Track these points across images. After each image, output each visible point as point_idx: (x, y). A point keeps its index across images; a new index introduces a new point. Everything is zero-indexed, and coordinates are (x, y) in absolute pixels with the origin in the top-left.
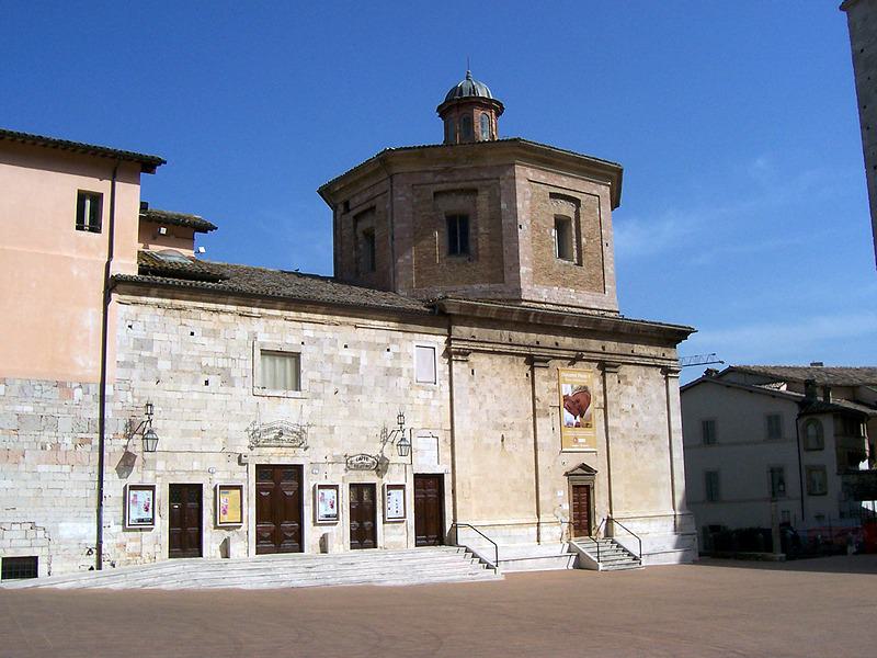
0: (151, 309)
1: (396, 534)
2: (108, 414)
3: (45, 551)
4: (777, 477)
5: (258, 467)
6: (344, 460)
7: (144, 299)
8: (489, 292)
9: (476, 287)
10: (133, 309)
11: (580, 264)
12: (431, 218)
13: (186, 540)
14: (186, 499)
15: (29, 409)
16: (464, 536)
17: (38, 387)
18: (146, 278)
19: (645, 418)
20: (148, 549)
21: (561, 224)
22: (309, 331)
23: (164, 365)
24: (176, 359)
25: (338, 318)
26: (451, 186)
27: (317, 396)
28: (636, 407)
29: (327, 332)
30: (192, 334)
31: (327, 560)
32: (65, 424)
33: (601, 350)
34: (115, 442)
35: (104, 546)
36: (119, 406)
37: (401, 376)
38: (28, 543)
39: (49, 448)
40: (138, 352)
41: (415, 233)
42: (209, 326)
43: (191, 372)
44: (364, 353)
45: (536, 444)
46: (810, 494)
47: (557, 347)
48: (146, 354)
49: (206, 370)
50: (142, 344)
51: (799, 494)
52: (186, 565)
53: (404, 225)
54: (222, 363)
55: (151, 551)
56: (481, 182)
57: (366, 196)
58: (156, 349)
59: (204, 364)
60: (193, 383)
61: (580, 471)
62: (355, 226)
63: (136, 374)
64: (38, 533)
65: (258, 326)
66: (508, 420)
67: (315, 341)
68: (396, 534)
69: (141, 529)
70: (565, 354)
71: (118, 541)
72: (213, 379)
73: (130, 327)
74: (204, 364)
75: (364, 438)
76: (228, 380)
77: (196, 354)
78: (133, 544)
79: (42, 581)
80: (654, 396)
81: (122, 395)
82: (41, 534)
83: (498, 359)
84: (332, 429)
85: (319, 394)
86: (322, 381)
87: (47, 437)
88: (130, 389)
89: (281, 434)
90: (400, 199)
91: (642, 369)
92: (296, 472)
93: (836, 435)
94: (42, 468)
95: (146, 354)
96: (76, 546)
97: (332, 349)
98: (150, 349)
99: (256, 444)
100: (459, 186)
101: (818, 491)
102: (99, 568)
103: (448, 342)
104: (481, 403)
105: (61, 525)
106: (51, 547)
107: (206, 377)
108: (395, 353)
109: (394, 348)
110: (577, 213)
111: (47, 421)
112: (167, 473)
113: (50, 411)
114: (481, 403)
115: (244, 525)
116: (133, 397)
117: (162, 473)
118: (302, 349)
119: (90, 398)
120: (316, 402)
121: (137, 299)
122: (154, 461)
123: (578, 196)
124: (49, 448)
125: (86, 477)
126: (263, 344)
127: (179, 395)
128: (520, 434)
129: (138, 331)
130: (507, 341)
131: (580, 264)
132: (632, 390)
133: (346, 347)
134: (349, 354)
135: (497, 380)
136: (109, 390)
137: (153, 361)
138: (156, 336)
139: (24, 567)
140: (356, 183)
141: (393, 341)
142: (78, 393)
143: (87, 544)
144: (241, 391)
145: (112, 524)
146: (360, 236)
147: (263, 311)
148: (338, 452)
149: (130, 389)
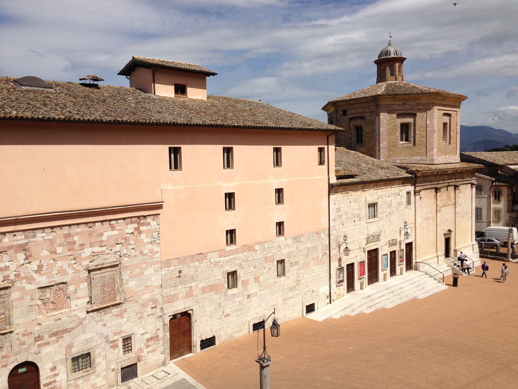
8: (420, 161)
9: (414, 158)
11: (450, 144)
14: (14, 236)
16: (422, 267)
19: (465, 206)
21: (445, 124)
23: (344, 217)
24: (346, 213)
26: (405, 112)
32: (320, 249)
38: (311, 298)
42: (355, 197)
45: (437, 224)
57: (360, 110)
67: (381, 196)
72: (356, 219)
82: (315, 293)
83: (427, 191)
91: (465, 185)
93: (508, 195)
94: (315, 268)
100: (408, 112)
102: (330, 303)
103: (415, 188)
110: (450, 121)
123: (449, 112)
128: (432, 221)
131: (450, 144)
132: (462, 195)
134: (389, 199)
135: (427, 200)
140: (353, 104)
144: (363, 222)
146: (352, 127)
148: (387, 240)
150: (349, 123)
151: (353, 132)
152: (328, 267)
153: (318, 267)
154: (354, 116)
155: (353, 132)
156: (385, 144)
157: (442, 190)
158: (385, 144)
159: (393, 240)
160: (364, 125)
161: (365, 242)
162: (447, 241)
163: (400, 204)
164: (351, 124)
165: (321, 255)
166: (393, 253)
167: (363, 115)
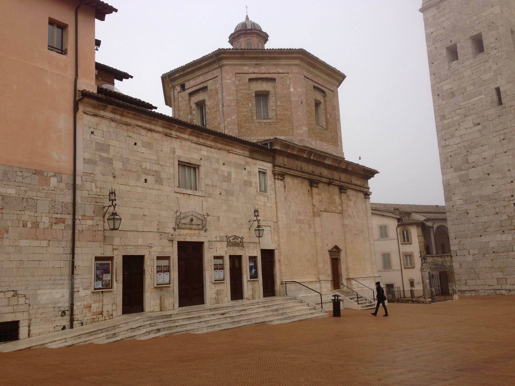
0: (107, 122)
1: (252, 288)
2: (78, 199)
3: (26, 315)
4: (386, 259)
5: (178, 242)
6: (225, 239)
7: (102, 113)
10: (94, 120)
12: (247, 94)
13: (133, 302)
14: (134, 266)
15: (11, 191)
17: (19, 174)
18: (100, 95)
20: (107, 308)
21: (317, 104)
22: (204, 152)
23: (118, 165)
24: (125, 161)
25: (219, 145)
27: (210, 195)
28: (354, 214)
29: (214, 154)
30: (135, 144)
31: (217, 310)
33: (339, 179)
34: (83, 222)
35: (75, 308)
36: (85, 193)
37: (252, 186)
38: (10, 309)
39: (29, 225)
40: (99, 153)
41: (237, 103)
42: (146, 139)
43: (136, 172)
44: (233, 170)
46: (405, 268)
47: (321, 176)
48: (105, 155)
49: (146, 172)
50: (103, 147)
51: (399, 268)
52: (135, 320)
53: (231, 98)
54: (155, 167)
55: (110, 309)
56: (278, 75)
58: (112, 153)
59: (144, 167)
60: (137, 181)
61: (334, 250)
62: (190, 100)
63: (98, 170)
64: (20, 299)
65: (176, 144)
66: (302, 217)
67: (208, 158)
68: (252, 288)
69: (102, 292)
70: (324, 180)
71: (85, 303)
72: (150, 179)
73: (92, 133)
74: (144, 167)
75: (235, 226)
76: (159, 181)
77: (138, 159)
78: (97, 305)
79: (23, 343)
80: (360, 208)
81: (88, 185)
82: (22, 300)
84: (218, 218)
85: (211, 194)
86: (213, 186)
87: (26, 216)
88: (93, 181)
89: (192, 220)
90: (228, 81)
92: (199, 246)
94: (23, 243)
95: (105, 155)
96: (51, 309)
97: (216, 164)
98: (108, 151)
99: (178, 226)
100: (264, 76)
101: (409, 266)
102: (72, 327)
104: (289, 207)
105: (39, 292)
106: (31, 312)
107: (145, 177)
108: (248, 171)
109: (248, 168)
111: (28, 203)
112: (121, 247)
113: (30, 194)
114: (289, 207)
115: (171, 285)
116: (96, 187)
117: (120, 248)
118: (202, 163)
119: (63, 186)
120: (210, 200)
121: (97, 112)
122: (112, 237)
123: (325, 90)
124: (29, 225)
125: (60, 251)
126: (179, 157)
127: (128, 188)
129: (98, 137)
130: (300, 170)
132: (351, 204)
133: (224, 164)
135: (296, 193)
136: (79, 181)
137: (109, 161)
138: (111, 143)
139: (8, 331)
141: (247, 163)
142: (54, 181)
143: (56, 307)
145: (81, 289)
146: (194, 106)
147: (178, 134)
148: (223, 234)
149: (93, 181)
150: (190, 100)
151: (194, 112)
152: (69, 251)
153: (36, 243)
154: (194, 89)
155: (194, 112)
156: (234, 117)
157: (321, 185)
158: (234, 117)
159: (236, 237)
160: (207, 98)
161: (173, 225)
162: (335, 262)
163: (248, 184)
164: (192, 102)
165: (46, 220)
166: (236, 261)
167: (205, 85)
